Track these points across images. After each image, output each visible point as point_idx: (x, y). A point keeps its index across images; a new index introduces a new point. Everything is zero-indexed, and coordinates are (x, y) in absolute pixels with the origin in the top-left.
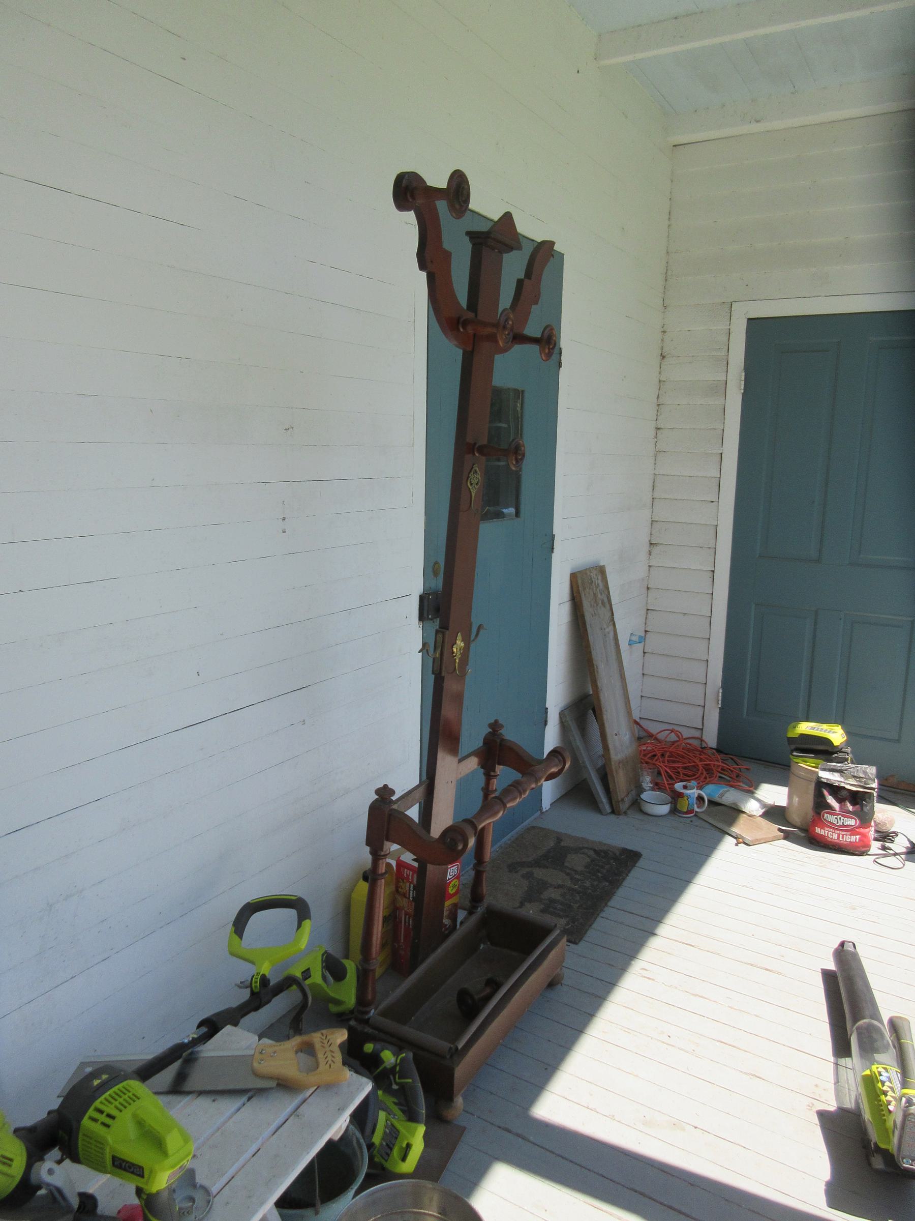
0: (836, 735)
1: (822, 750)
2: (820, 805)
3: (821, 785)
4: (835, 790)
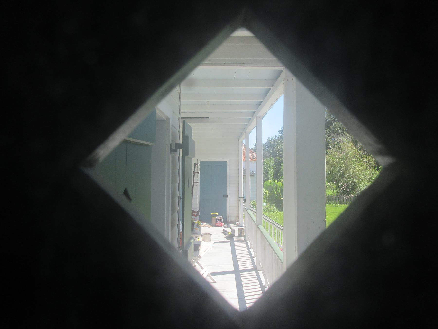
0: (217, 214)
1: (216, 215)
2: (217, 222)
3: (217, 219)
4: (218, 219)
